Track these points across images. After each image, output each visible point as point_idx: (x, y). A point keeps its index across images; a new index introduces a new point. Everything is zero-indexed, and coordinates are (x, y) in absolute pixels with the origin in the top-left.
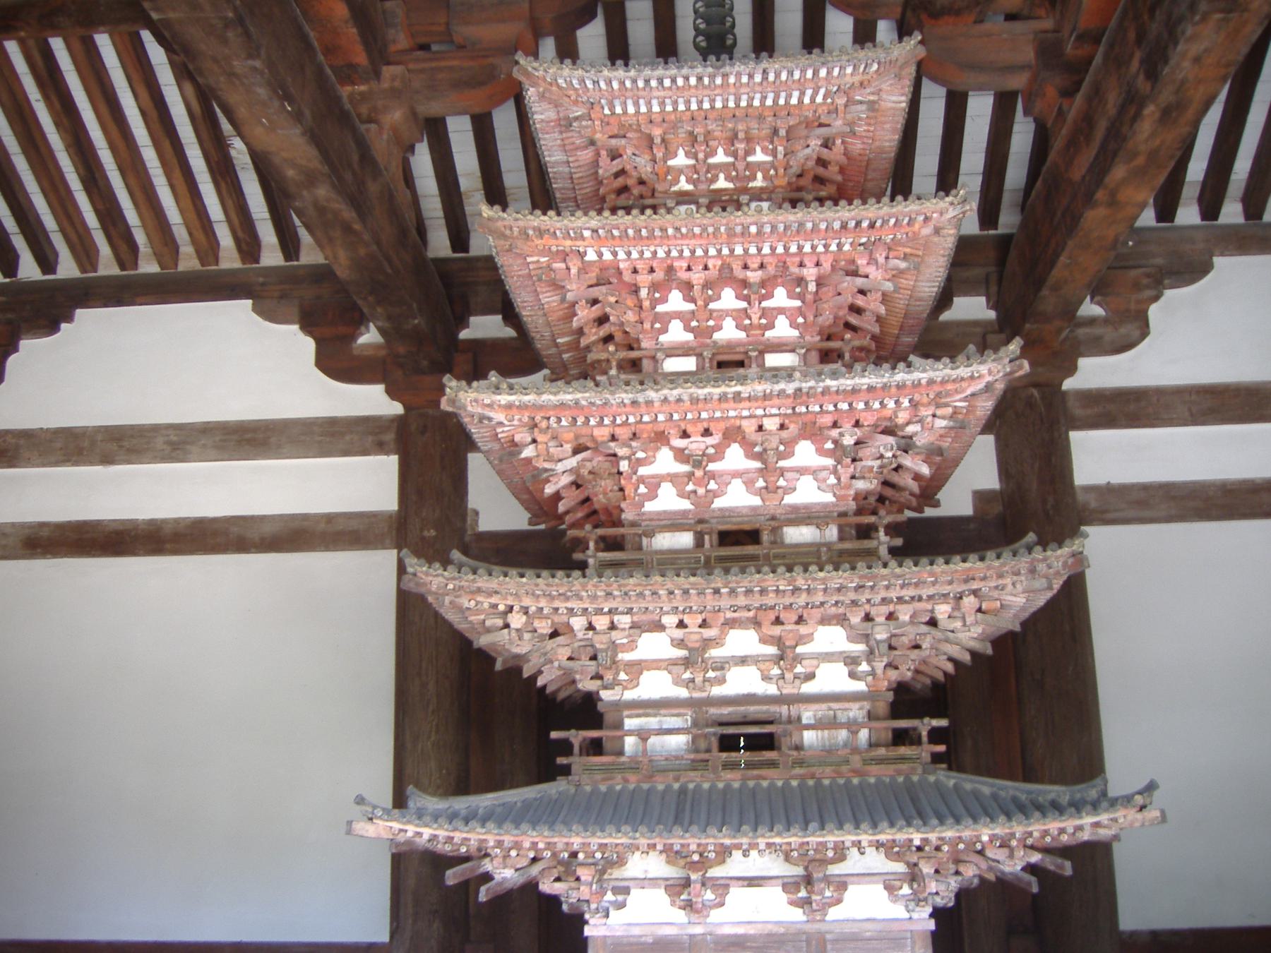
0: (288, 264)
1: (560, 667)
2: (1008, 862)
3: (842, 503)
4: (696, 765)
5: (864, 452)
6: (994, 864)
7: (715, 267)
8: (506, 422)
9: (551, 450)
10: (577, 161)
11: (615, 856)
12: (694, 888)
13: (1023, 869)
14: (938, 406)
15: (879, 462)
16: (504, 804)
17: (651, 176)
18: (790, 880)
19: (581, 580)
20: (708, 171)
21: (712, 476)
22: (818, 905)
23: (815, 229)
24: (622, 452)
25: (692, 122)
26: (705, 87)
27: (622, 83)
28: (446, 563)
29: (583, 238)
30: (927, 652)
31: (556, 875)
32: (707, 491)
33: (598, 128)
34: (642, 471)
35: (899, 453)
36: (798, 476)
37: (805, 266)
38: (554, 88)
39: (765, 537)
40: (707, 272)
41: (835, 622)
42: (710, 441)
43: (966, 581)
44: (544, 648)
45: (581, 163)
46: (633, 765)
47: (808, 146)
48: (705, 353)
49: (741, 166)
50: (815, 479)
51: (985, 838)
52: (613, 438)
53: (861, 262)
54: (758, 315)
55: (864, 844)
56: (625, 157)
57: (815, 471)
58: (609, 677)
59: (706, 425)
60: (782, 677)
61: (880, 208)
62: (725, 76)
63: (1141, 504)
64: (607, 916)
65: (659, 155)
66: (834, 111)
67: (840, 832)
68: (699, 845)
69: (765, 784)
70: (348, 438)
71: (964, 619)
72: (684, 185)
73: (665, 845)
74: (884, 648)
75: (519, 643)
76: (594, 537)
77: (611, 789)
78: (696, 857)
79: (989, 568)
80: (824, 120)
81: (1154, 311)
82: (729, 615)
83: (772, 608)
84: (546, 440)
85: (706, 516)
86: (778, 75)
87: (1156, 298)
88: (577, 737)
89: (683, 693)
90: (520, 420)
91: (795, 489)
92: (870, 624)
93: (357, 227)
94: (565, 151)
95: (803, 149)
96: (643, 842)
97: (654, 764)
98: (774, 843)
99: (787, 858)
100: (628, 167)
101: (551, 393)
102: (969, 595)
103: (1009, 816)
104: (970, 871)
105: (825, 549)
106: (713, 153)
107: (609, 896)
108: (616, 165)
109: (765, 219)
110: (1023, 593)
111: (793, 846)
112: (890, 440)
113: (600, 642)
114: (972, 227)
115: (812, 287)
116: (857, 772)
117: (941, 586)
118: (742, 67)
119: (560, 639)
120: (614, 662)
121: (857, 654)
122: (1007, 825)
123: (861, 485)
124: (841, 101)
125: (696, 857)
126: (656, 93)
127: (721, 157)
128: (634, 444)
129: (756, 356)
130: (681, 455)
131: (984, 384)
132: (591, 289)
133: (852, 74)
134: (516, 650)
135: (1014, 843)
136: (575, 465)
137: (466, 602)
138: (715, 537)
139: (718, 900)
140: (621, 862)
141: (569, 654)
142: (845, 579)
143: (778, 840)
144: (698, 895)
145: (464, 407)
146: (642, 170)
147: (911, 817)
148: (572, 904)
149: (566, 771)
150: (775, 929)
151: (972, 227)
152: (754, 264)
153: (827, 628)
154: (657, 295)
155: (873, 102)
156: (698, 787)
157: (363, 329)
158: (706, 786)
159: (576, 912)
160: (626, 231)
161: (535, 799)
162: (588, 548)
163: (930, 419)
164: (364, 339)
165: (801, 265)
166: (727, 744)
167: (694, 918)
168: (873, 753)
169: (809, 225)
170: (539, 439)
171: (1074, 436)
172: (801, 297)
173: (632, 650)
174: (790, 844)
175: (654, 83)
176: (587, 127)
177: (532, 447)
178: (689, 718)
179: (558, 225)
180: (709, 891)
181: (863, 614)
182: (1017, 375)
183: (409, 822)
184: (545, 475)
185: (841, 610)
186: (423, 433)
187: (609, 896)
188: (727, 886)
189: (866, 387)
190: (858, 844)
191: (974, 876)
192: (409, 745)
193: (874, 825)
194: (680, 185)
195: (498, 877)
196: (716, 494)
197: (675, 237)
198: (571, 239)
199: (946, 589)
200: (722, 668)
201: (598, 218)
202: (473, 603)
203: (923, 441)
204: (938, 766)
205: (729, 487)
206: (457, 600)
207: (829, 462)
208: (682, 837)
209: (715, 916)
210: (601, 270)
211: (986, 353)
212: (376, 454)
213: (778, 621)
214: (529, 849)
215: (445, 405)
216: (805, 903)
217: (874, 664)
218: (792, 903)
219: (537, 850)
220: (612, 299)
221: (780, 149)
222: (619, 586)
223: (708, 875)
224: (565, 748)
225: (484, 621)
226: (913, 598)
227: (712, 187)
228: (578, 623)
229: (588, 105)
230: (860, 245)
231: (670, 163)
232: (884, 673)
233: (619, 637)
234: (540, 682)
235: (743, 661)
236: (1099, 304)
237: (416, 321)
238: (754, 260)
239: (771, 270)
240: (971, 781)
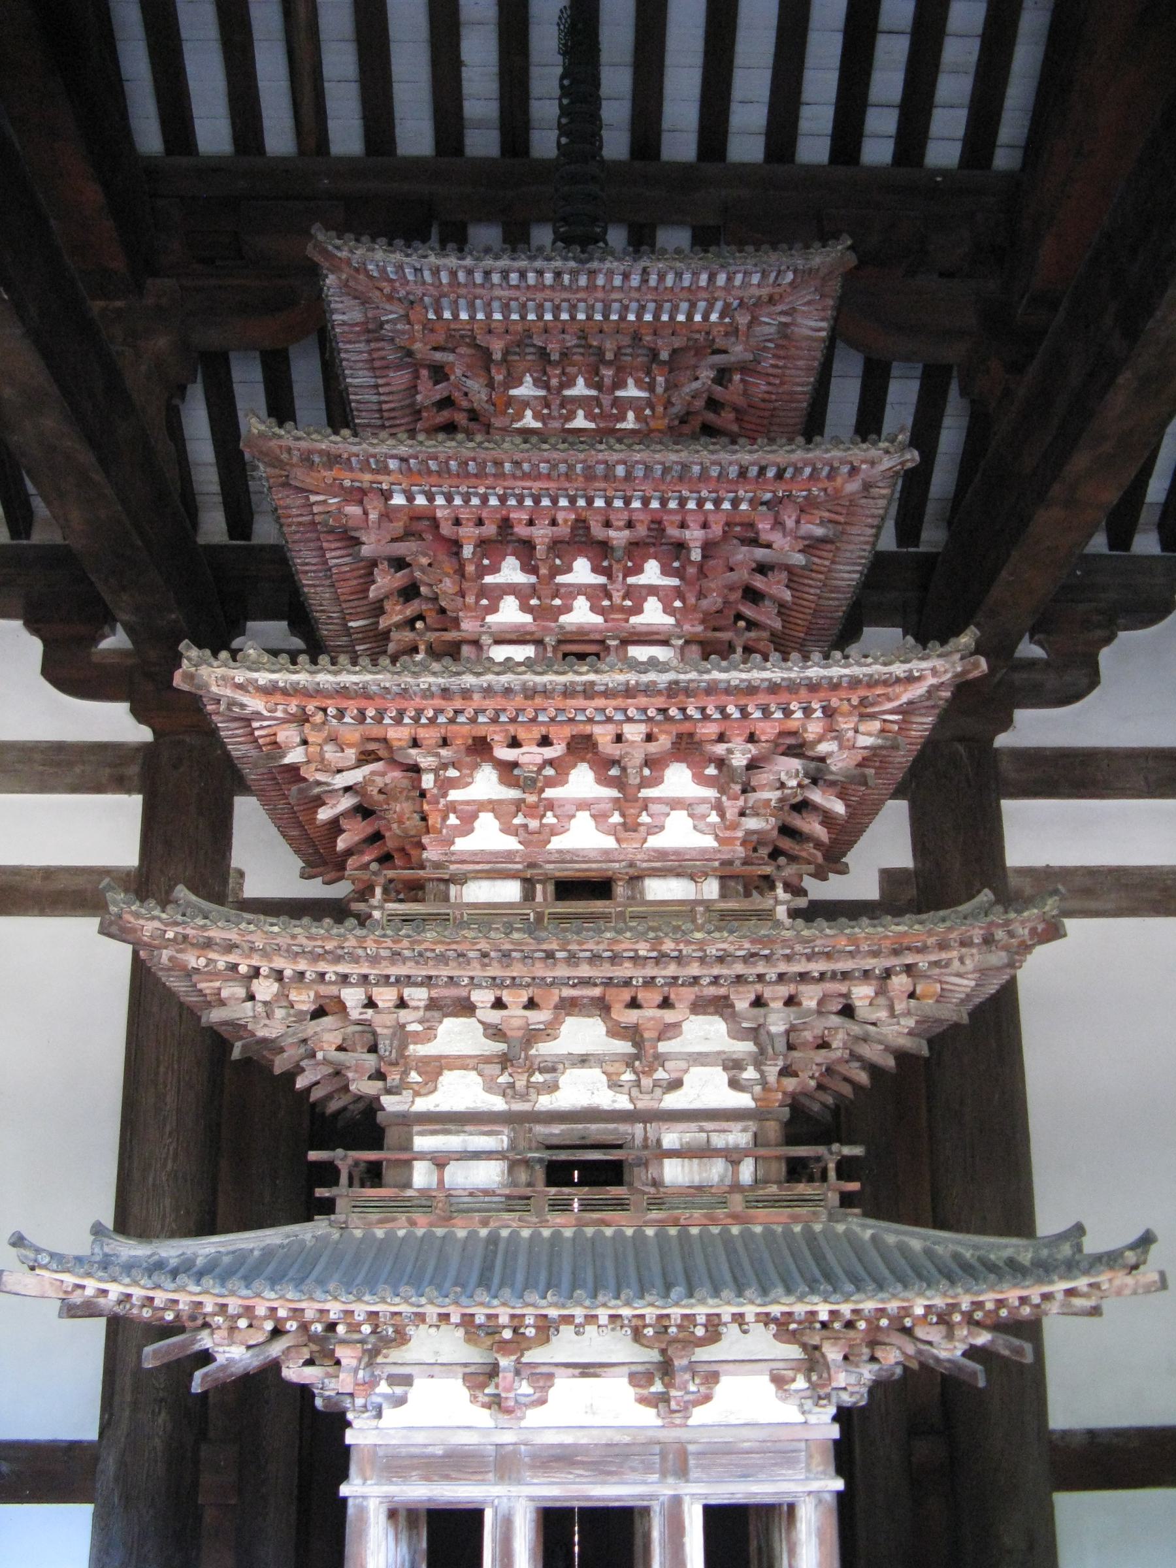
0: (15, 542)
1: (326, 1061)
2: (945, 1344)
3: (725, 848)
4: (516, 1202)
5: (762, 777)
6: (926, 1347)
7: (566, 521)
8: (266, 713)
9: (327, 756)
10: (387, 384)
11: (390, 1330)
12: (505, 1378)
13: (964, 1354)
14: (863, 717)
15: (778, 794)
16: (233, 1252)
17: (486, 406)
18: (640, 1368)
19: (359, 932)
20: (562, 406)
21: (550, 805)
22: (678, 1404)
23: (704, 476)
24: (425, 761)
25: (545, 336)
26: (565, 288)
27: (453, 274)
28: (165, 902)
29: (386, 471)
30: (839, 1053)
31: (308, 1357)
32: (542, 825)
33: (418, 335)
34: (454, 795)
35: (807, 781)
36: (667, 809)
37: (688, 527)
38: (361, 277)
39: (620, 890)
40: (555, 528)
41: (712, 1009)
42: (549, 753)
43: (896, 952)
44: (305, 1030)
45: (394, 389)
46: (424, 1203)
47: (697, 379)
48: (547, 639)
49: (606, 400)
50: (691, 815)
51: (919, 1311)
52: (415, 743)
53: (764, 526)
54: (621, 594)
55: (750, 1318)
56: (452, 378)
57: (690, 805)
58: (394, 1077)
59: (544, 731)
60: (638, 1084)
61: (792, 451)
62: (592, 273)
63: (1087, 892)
64: (379, 1415)
65: (499, 378)
66: (733, 331)
67: (716, 1301)
68: (513, 1316)
69: (609, 1232)
70: (78, 770)
71: (891, 1008)
72: (529, 420)
73: (463, 1315)
74: (781, 1045)
75: (267, 1022)
76: (382, 880)
77: (390, 1235)
78: (507, 1334)
79: (930, 933)
80: (720, 343)
81: (1105, 656)
82: (567, 992)
83: (627, 983)
84: (320, 741)
85: (540, 859)
86: (662, 277)
87: (1108, 640)
88: (345, 1159)
89: (498, 1104)
90: (285, 711)
91: (662, 828)
92: (761, 1011)
93: (98, 477)
94: (373, 369)
95: (690, 381)
96: (432, 1311)
97: (454, 1200)
98: (620, 1316)
99: (637, 1335)
100: (457, 395)
101: (329, 672)
102: (901, 972)
103: (952, 1280)
104: (891, 1357)
105: (701, 909)
106: (571, 383)
107: (383, 1388)
108: (441, 391)
109: (638, 457)
110: (974, 972)
111: (648, 1321)
112: (795, 764)
113: (383, 1023)
114: (888, 542)
115: (696, 555)
116: (736, 1218)
117: (864, 958)
118: (616, 264)
119: (326, 1021)
120: (403, 1056)
121: (740, 1056)
122: (951, 1292)
123: (752, 823)
124: (743, 320)
125: (507, 1334)
126: (498, 292)
127: (580, 389)
128: (444, 752)
129: (617, 647)
130: (507, 770)
131: (924, 689)
132: (396, 544)
133: (759, 285)
134: (261, 1033)
135: (957, 1318)
136: (361, 779)
137: (194, 960)
138: (551, 888)
139: (537, 1395)
140: (401, 1338)
141: (339, 1041)
142: (732, 943)
143: (626, 1312)
144: (509, 1389)
145: (206, 686)
146: (475, 398)
147: (816, 1281)
148: (329, 1397)
149: (327, 1207)
150: (618, 1438)
151: (888, 542)
152: (619, 520)
153: (701, 1018)
154: (486, 562)
155: (786, 325)
156: (514, 1235)
157: (107, 629)
158: (526, 1233)
159: (335, 1410)
160: (447, 463)
161: (282, 1246)
162: (373, 896)
163: (851, 734)
164: (105, 644)
165: (683, 525)
166: (557, 1174)
167: (504, 1420)
168: (761, 1192)
169: (696, 469)
170: (310, 740)
171: (1007, 805)
172: (678, 573)
173: (429, 1040)
174: (642, 1317)
175: (496, 278)
176: (403, 332)
177: (301, 749)
178: (505, 1139)
179: (355, 449)
180: (524, 1382)
181: (752, 997)
182: (971, 676)
183: (89, 1275)
184: (317, 790)
185: (722, 991)
186: (175, 767)
187: (383, 1388)
188: (550, 1376)
189: (766, 684)
190: (739, 1318)
191: (897, 1363)
192: (136, 1175)
193: (764, 1291)
194: (525, 421)
195: (221, 1359)
196: (554, 832)
197: (514, 477)
198: (373, 471)
199: (869, 963)
200: (553, 1070)
201: (410, 442)
202: (202, 961)
203: (840, 765)
204: (849, 1211)
205: (573, 821)
206: (179, 956)
207: (711, 793)
208: (488, 1306)
209: (534, 1417)
210: (411, 519)
211: (930, 645)
212: (114, 791)
213: (634, 1004)
214: (266, 1318)
215: (178, 681)
216: (659, 1401)
217: (764, 1068)
218: (642, 1400)
219: (278, 1320)
220: (424, 561)
221: (660, 379)
222: (412, 943)
223: (524, 1360)
224: (328, 1174)
225: (220, 989)
226: (822, 975)
227: (567, 426)
228: (352, 997)
229: (406, 304)
230: (762, 504)
231: (514, 392)
232: (778, 1082)
233: (410, 1019)
234: (301, 1083)
235: (583, 1061)
236: (1040, 644)
237: (173, 616)
238: (620, 516)
239: (642, 531)
240: (897, 1232)
